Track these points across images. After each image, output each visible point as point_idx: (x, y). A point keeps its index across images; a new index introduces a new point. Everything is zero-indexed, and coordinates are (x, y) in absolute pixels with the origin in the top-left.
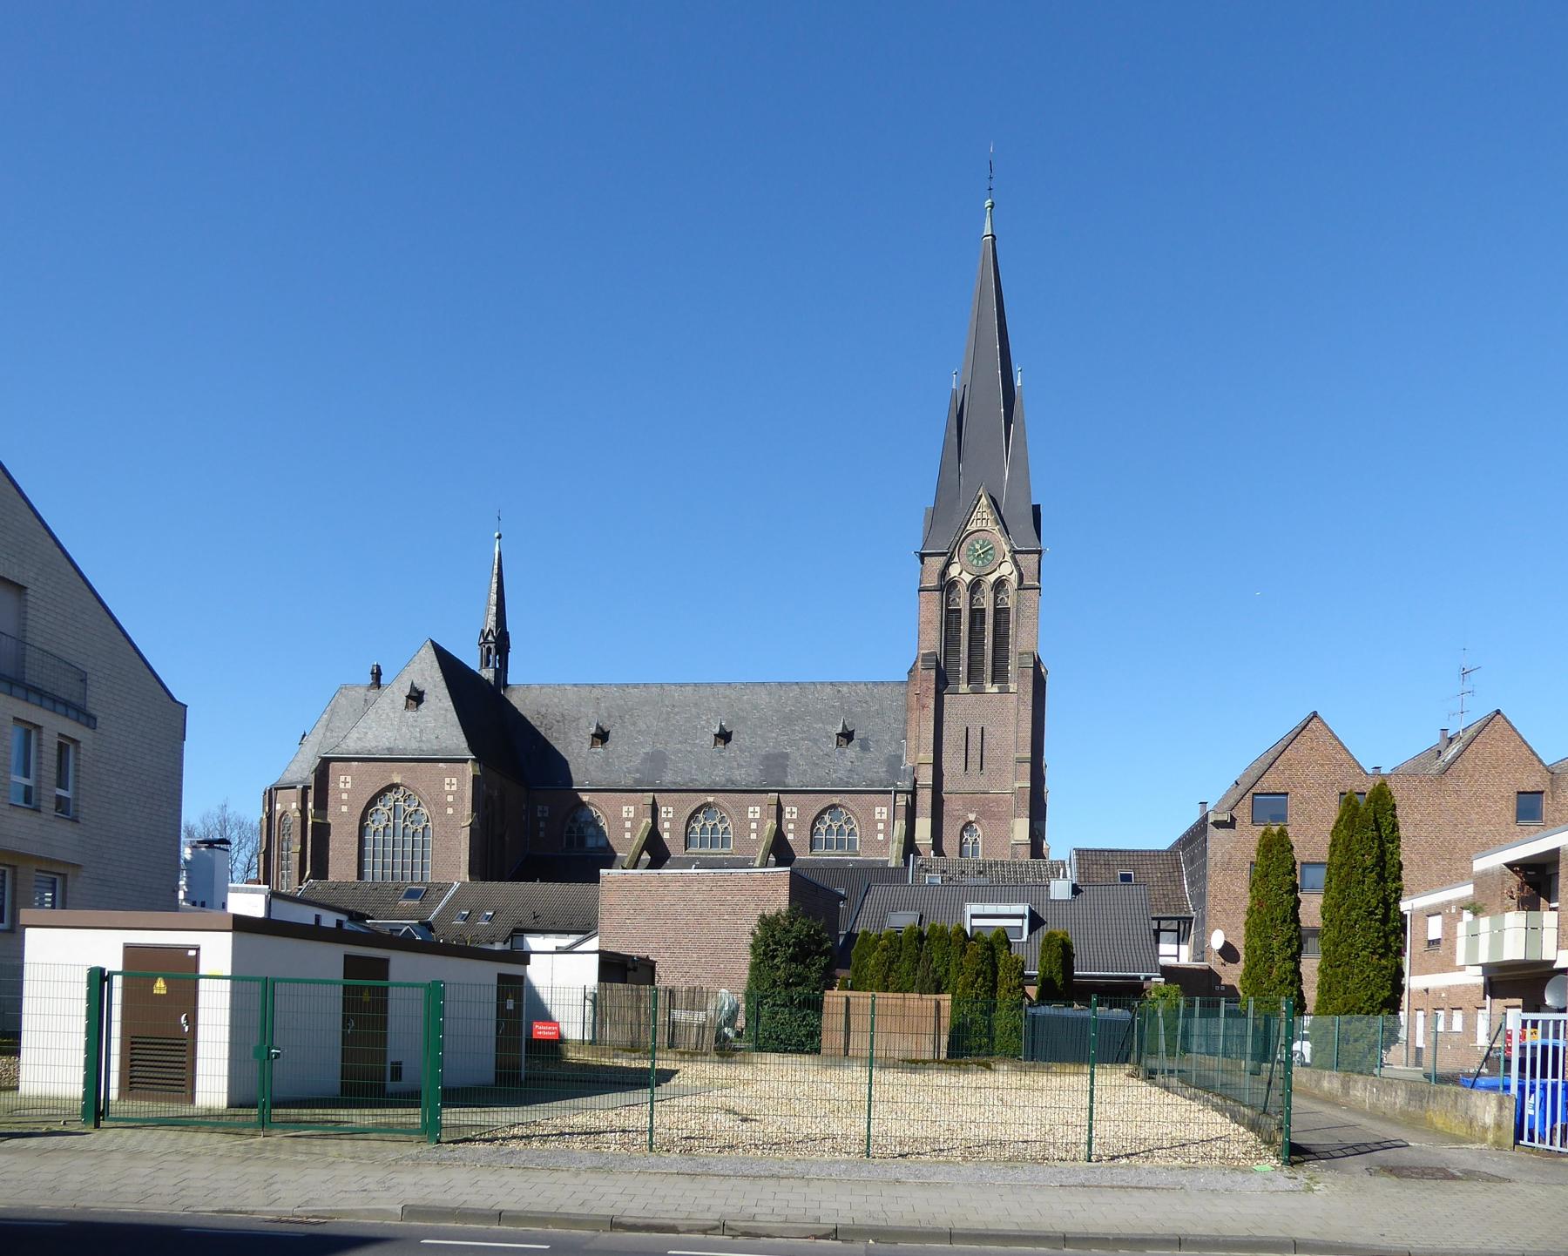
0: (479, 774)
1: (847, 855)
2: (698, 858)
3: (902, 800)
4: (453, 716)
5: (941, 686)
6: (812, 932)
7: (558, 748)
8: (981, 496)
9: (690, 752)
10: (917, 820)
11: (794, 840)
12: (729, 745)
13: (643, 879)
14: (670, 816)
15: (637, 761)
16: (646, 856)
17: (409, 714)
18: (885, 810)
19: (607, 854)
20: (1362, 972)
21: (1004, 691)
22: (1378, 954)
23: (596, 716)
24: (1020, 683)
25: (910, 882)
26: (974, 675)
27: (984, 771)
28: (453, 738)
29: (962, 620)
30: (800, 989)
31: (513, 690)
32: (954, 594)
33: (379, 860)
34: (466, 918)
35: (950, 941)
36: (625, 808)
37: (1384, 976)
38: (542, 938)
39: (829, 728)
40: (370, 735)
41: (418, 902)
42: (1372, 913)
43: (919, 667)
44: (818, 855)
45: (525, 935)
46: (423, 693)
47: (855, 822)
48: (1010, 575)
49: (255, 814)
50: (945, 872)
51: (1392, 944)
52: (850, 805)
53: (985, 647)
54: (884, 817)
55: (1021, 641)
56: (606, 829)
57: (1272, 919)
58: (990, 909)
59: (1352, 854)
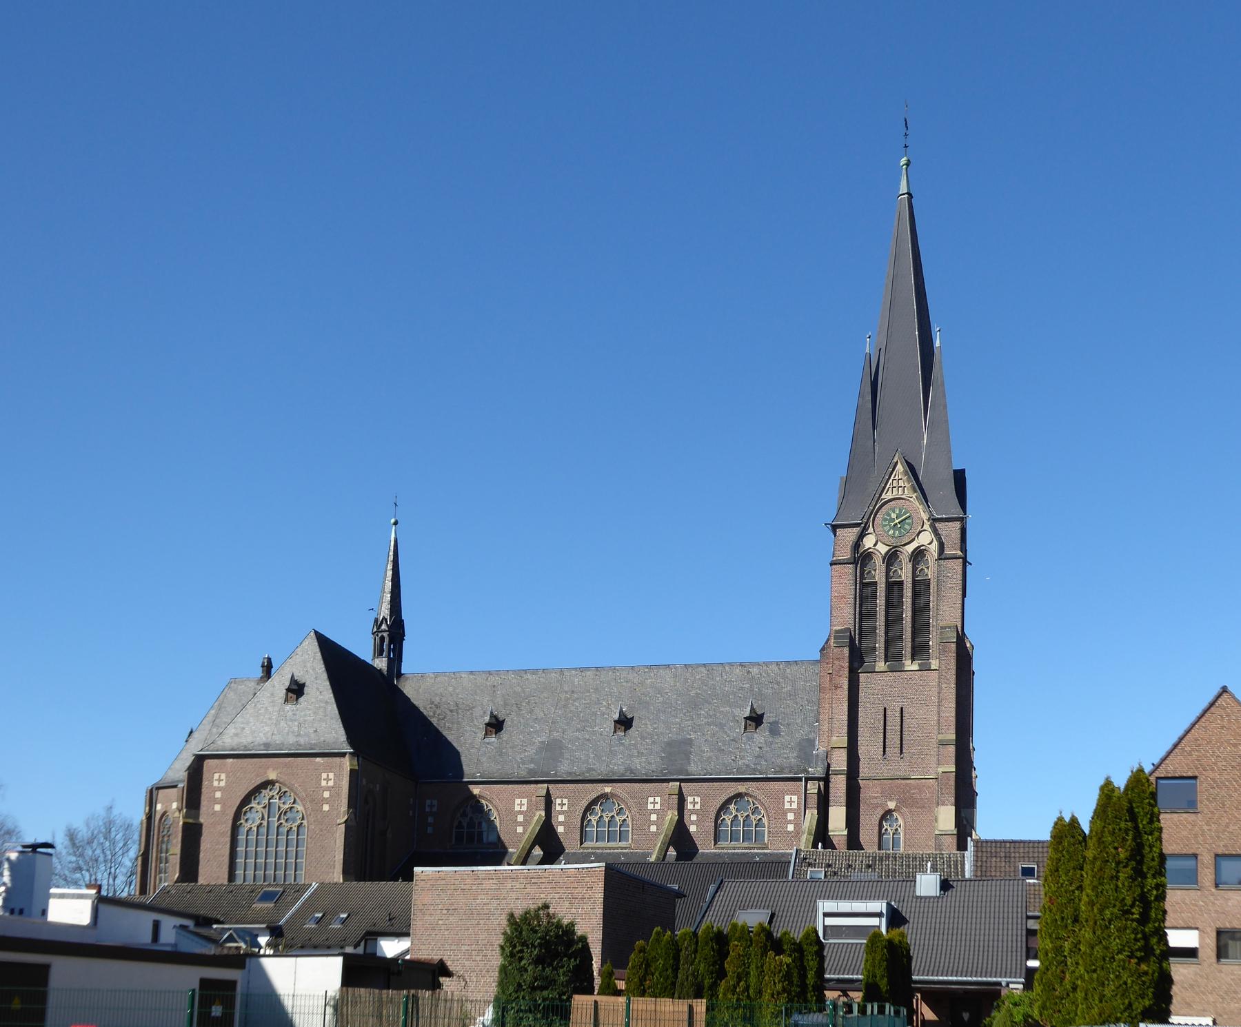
0: (357, 768)
1: (754, 848)
2: (593, 853)
3: (813, 788)
4: (333, 709)
5: (856, 665)
6: (560, 933)
7: (450, 738)
8: (897, 462)
9: (588, 740)
10: (830, 808)
11: (697, 832)
12: (630, 732)
13: (457, 877)
14: (565, 808)
15: (532, 751)
16: (538, 852)
17: (288, 707)
18: (795, 798)
19: (498, 850)
20: (1118, 977)
21: (925, 668)
22: (1137, 958)
23: (491, 704)
24: (942, 662)
25: (790, 878)
26: (892, 653)
27: (905, 755)
28: (333, 732)
29: (878, 594)
30: (545, 993)
31: (407, 679)
32: (869, 566)
33: (251, 861)
34: (319, 921)
35: (751, 941)
36: (517, 801)
37: (1144, 983)
38: (397, 941)
39: (737, 711)
40: (247, 730)
41: (272, 905)
42: (1128, 912)
43: (832, 644)
44: (723, 848)
45: (379, 938)
46: (303, 685)
47: (763, 812)
48: (930, 544)
49: (138, 815)
50: (829, 866)
51: (1155, 947)
52: (757, 793)
53: (904, 622)
54: (795, 806)
55: (943, 613)
56: (497, 823)
57: (1063, 918)
58: (845, 906)
59: (1105, 847)
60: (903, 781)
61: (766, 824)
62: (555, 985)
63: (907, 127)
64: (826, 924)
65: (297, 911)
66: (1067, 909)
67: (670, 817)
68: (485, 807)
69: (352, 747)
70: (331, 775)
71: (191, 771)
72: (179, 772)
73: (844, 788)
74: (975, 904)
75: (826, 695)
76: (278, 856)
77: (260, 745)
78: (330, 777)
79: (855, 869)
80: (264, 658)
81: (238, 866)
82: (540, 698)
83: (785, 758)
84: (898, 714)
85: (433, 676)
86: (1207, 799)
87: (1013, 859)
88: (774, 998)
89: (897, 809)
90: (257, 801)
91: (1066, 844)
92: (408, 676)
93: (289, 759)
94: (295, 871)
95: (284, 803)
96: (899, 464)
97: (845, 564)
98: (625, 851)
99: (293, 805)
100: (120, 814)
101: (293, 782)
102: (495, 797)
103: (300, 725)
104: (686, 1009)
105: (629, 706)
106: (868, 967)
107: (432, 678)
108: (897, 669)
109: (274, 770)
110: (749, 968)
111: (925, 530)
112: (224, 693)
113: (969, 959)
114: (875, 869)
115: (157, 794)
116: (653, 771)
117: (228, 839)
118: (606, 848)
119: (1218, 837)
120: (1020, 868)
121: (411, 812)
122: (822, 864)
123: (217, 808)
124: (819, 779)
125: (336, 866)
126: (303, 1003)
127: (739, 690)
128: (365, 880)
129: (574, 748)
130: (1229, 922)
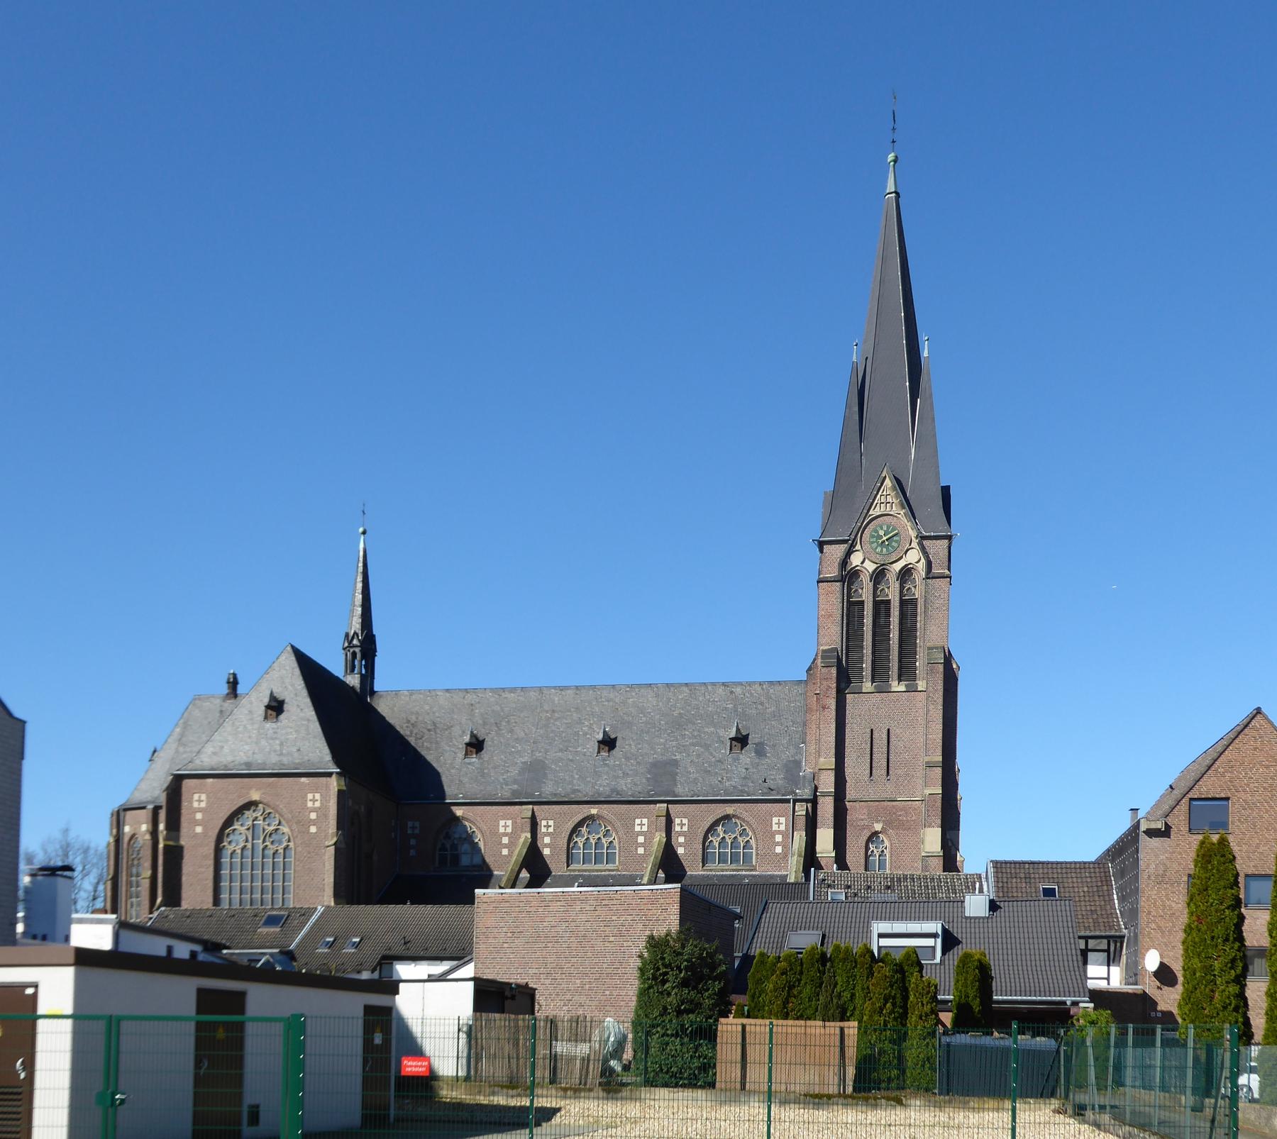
2: (580, 876)
3: (801, 810)
4: (316, 727)
5: (843, 685)
6: (705, 955)
7: (430, 758)
9: (571, 760)
12: (614, 752)
14: (551, 830)
15: (514, 772)
16: (525, 874)
17: (269, 725)
18: (783, 820)
21: (912, 689)
24: (928, 682)
25: (811, 899)
26: (879, 673)
28: (317, 751)
29: (865, 613)
33: (236, 884)
34: (331, 945)
36: (502, 823)
38: (413, 965)
39: (721, 732)
40: (226, 750)
41: (278, 929)
43: (819, 664)
44: (711, 870)
45: (395, 962)
47: (750, 833)
48: (917, 562)
49: (101, 838)
50: (849, 887)
52: (745, 815)
53: (891, 642)
54: (783, 828)
55: (929, 635)
56: (481, 845)
57: (1213, 938)
58: (899, 927)
60: (889, 803)
61: (754, 846)
62: (701, 1008)
63: (894, 121)
64: (880, 945)
65: (303, 939)
66: (1217, 928)
67: (658, 839)
68: (469, 829)
69: (339, 767)
70: (318, 796)
71: (170, 791)
72: (153, 789)
73: (832, 810)
74: (1016, 924)
75: (813, 715)
76: (265, 880)
77: (241, 764)
78: (316, 798)
79: (874, 890)
80: (230, 674)
81: (223, 890)
82: (519, 717)
83: (772, 779)
84: (885, 736)
85: (408, 693)
86: (1239, 820)
87: (1033, 880)
88: (922, 1019)
89: (883, 831)
90: (240, 823)
91: (1216, 862)
92: (382, 693)
93: (273, 779)
94: (283, 895)
95: (269, 825)
96: (887, 478)
97: (832, 581)
98: (612, 873)
99: (278, 827)
100: (78, 836)
101: (277, 803)
102: (478, 819)
103: (281, 744)
104: (740, 1028)
105: (612, 726)
106: (960, 987)
107: (407, 695)
108: (883, 689)
109: (257, 790)
110: (853, 989)
111: (912, 548)
112: (188, 710)
113: (1072, 979)
114: (894, 890)
115: (124, 817)
116: (639, 793)
117: (211, 862)
118: (593, 871)
119: (1249, 857)
120: (1041, 889)
121: (393, 834)
122: (841, 885)
123: (199, 829)
124: (806, 801)
125: (326, 890)
126: (433, 1030)
127: (723, 710)
128: (359, 903)
129: (558, 769)
130: (1256, 941)
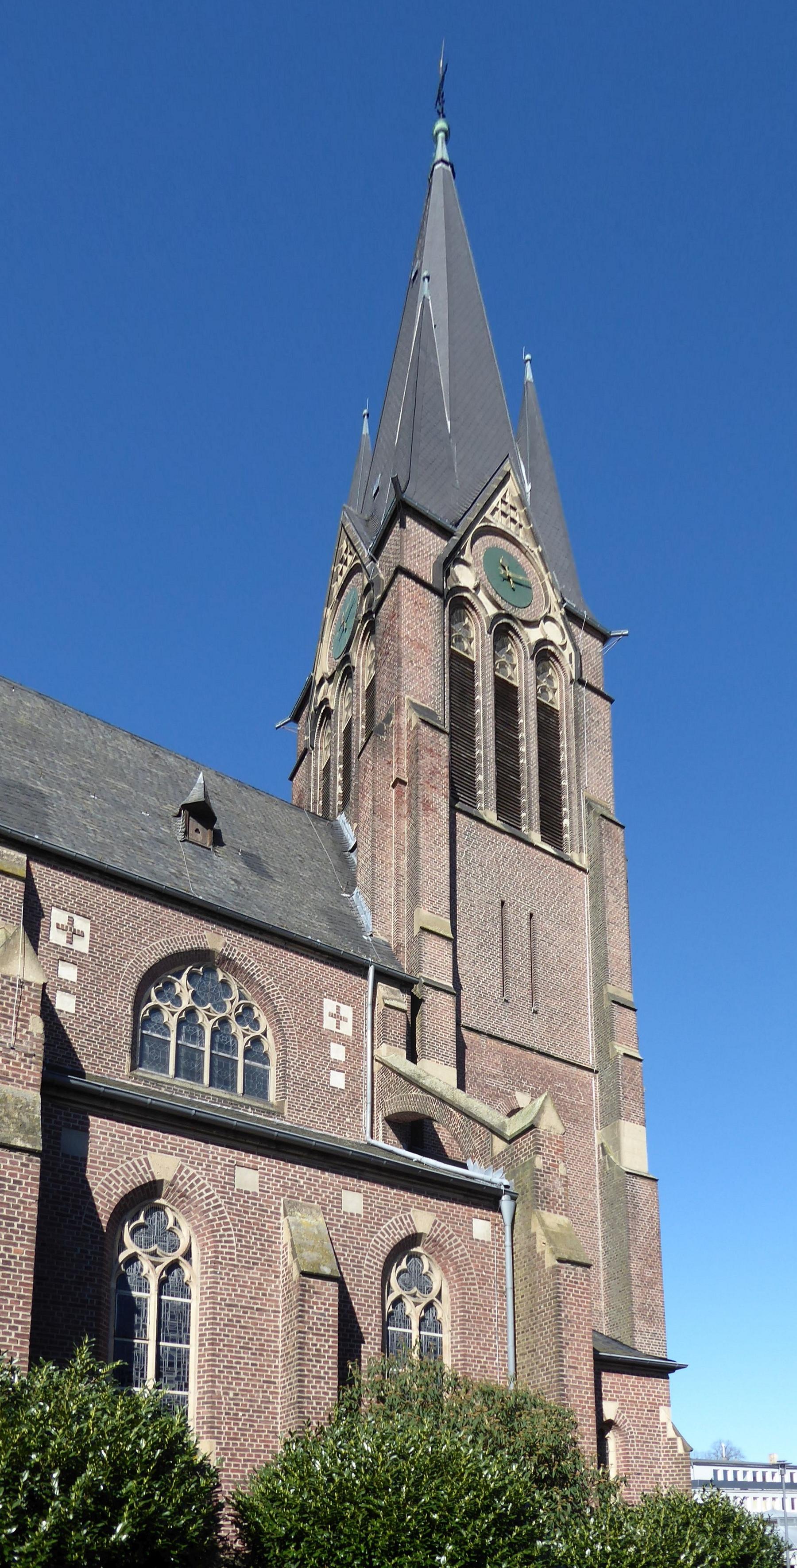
47: (263, 1022)
